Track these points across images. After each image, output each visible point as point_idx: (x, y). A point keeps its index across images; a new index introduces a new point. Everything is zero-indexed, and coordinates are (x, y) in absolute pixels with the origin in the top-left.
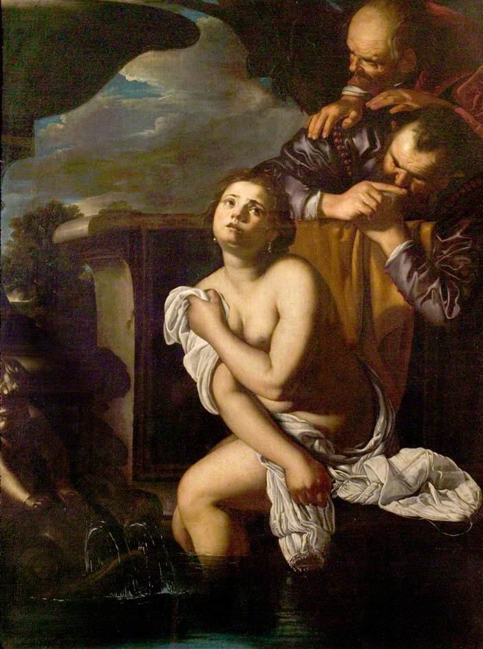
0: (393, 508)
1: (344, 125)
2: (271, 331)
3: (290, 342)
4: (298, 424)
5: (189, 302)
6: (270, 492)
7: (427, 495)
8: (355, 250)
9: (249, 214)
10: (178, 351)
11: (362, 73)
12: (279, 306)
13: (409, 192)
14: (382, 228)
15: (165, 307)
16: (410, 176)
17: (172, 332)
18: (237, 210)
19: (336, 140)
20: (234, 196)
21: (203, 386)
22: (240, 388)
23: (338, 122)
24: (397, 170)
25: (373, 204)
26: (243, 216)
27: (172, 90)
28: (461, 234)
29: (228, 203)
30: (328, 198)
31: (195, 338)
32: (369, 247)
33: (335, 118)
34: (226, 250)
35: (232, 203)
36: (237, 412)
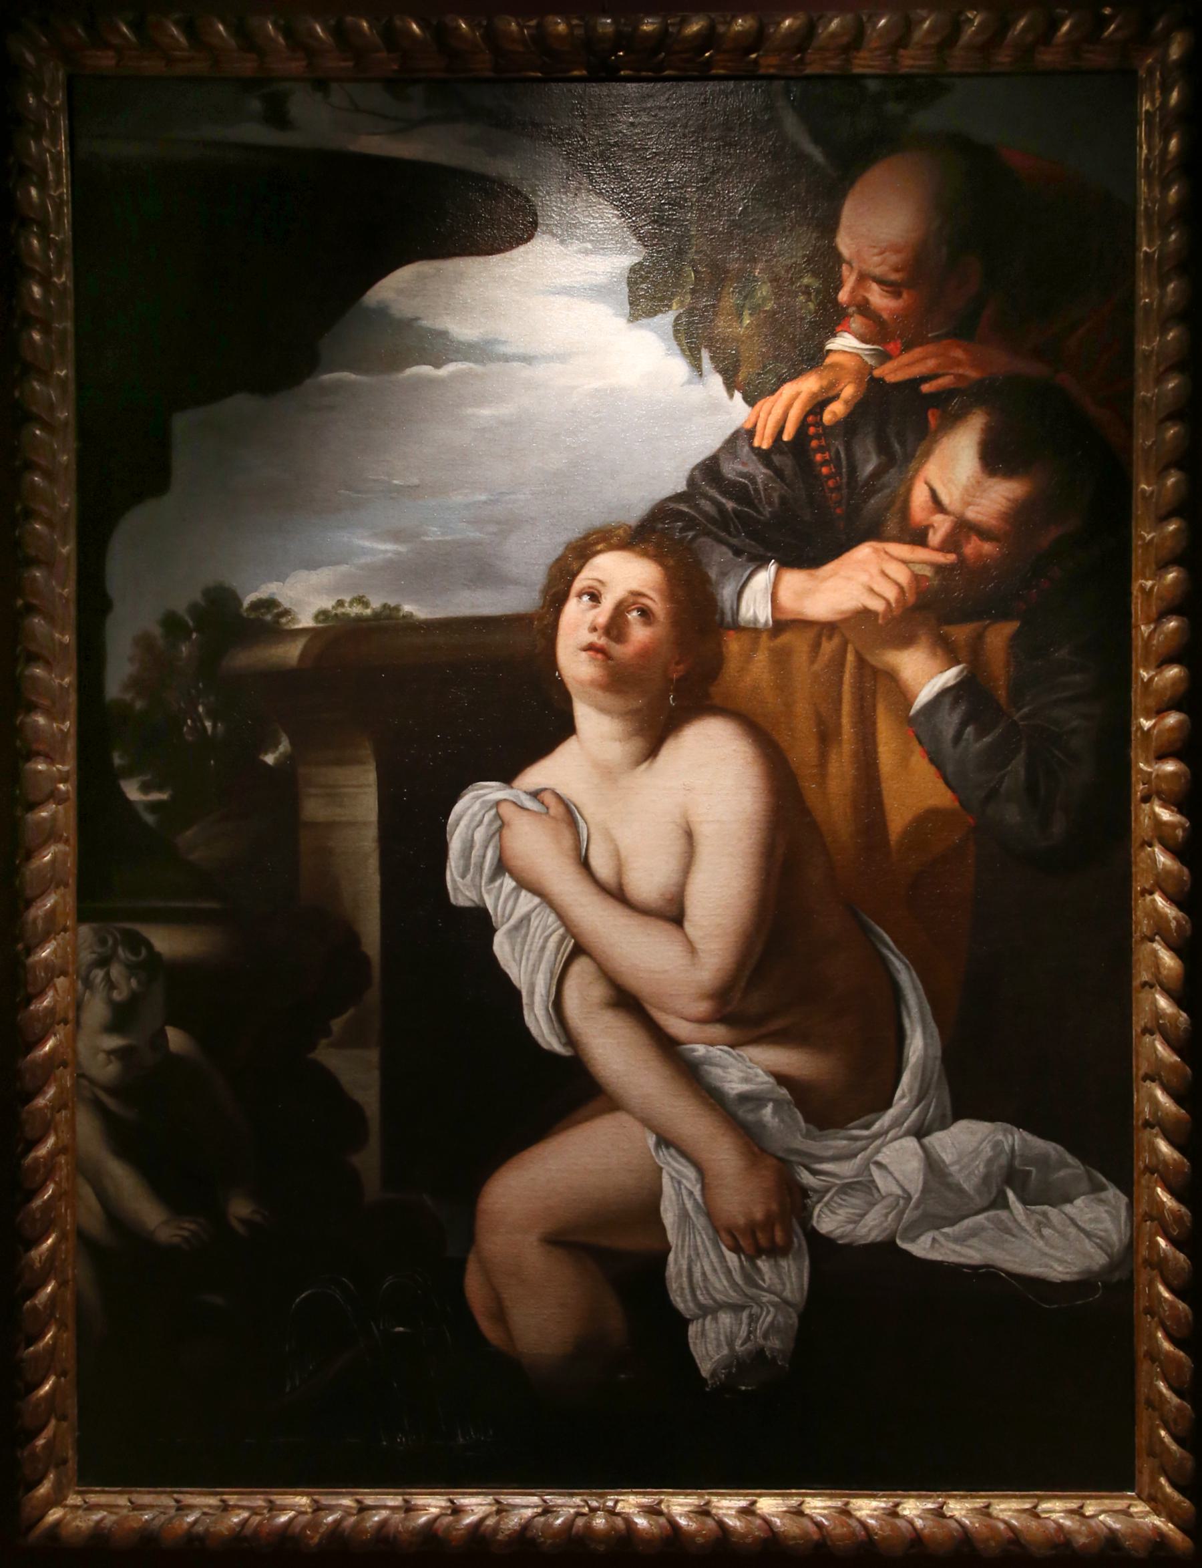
0: (921, 1248)
1: (827, 417)
2: (675, 877)
3: (721, 893)
4: (743, 1069)
5: (498, 816)
6: (669, 1217)
7: (1003, 1214)
8: (847, 677)
9: (627, 621)
10: (479, 923)
11: (864, 308)
12: (694, 819)
13: (962, 559)
14: (906, 641)
16: (963, 528)
19: (814, 443)
20: (600, 581)
21: (538, 999)
22: (626, 1001)
23: (818, 405)
24: (938, 518)
25: (891, 593)
26: (615, 628)
28: (734, 510)
29: (586, 598)
30: (794, 580)
32: (877, 684)
33: (814, 395)
35: (595, 597)
36: (613, 1050)
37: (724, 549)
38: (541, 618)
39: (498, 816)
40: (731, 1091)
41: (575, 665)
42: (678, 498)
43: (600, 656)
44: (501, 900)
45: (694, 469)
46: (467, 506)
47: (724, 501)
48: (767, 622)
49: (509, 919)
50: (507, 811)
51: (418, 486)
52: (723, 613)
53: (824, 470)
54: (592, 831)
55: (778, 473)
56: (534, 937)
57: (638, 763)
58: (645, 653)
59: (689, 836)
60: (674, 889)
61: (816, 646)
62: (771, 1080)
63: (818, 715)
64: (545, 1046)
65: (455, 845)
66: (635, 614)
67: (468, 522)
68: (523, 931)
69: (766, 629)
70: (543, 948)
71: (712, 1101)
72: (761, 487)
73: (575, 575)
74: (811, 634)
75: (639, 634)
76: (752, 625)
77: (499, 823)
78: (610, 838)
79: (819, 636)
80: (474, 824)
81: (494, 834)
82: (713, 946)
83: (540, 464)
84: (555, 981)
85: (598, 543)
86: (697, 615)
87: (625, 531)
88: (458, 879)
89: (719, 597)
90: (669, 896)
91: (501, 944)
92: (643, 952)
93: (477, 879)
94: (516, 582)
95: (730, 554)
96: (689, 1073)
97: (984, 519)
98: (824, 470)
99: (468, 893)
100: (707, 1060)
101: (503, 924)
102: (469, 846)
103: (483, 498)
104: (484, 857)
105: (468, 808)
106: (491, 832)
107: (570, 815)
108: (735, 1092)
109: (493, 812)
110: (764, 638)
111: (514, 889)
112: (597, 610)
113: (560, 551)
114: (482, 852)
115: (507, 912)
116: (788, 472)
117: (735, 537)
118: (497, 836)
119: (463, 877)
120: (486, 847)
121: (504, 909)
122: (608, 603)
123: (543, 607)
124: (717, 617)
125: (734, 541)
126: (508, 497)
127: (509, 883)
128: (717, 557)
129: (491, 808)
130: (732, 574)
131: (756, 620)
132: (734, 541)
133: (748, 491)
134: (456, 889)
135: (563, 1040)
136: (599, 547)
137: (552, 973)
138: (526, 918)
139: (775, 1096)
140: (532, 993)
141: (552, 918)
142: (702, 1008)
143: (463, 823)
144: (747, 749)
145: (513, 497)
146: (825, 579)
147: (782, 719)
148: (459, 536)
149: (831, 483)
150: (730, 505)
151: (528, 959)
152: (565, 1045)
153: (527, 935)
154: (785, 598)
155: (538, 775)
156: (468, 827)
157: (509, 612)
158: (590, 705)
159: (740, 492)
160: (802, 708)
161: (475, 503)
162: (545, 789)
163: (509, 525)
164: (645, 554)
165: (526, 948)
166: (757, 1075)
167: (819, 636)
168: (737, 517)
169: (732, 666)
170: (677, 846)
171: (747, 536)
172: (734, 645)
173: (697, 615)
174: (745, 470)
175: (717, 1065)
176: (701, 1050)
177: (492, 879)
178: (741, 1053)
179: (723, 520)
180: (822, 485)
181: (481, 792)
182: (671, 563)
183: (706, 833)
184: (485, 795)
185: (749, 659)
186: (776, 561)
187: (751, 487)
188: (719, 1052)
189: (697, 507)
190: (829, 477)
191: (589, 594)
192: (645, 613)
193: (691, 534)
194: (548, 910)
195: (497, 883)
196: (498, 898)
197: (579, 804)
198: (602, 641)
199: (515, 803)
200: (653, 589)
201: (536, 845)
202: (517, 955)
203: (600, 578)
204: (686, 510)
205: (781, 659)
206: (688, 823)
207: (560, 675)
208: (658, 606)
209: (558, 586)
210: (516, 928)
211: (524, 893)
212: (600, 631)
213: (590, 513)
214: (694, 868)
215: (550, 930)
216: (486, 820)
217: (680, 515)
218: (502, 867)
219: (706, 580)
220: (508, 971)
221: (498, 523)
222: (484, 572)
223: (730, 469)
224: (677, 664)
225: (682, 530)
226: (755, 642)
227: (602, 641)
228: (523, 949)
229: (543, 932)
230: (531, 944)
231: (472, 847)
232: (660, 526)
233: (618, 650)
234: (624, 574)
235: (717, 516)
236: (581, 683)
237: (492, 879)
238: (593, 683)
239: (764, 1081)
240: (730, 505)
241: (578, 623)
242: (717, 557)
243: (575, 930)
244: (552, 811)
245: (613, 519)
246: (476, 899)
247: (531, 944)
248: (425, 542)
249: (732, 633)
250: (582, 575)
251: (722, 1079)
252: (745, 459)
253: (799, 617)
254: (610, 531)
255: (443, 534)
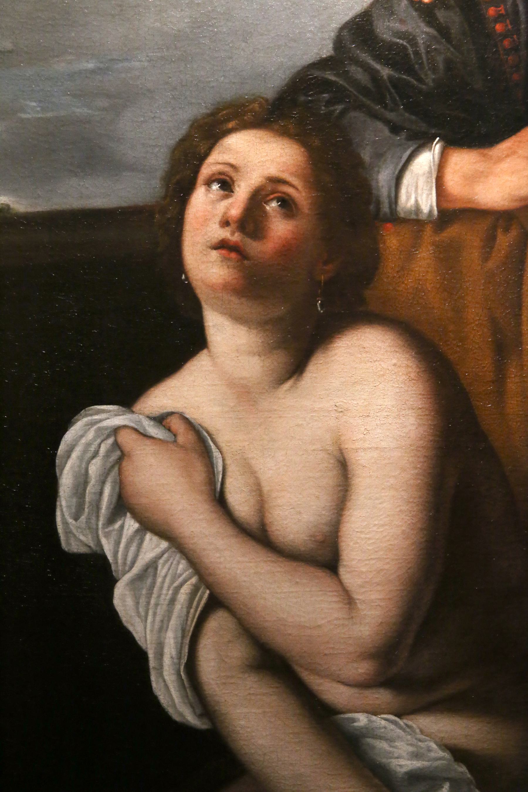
2: (327, 516)
3: (381, 531)
5: (116, 445)
10: (97, 572)
12: (348, 445)
15: (58, 475)
17: (78, 524)
18: (236, 204)
20: (232, 166)
21: (167, 661)
26: (252, 220)
27: (217, 409)
28: (390, 78)
29: (215, 187)
30: (463, 161)
31: (153, 668)
34: (215, 308)
35: (227, 185)
37: (379, 125)
38: (163, 211)
39: (116, 445)
40: (399, 769)
41: (204, 266)
42: (322, 64)
43: (233, 255)
44: (122, 545)
45: (342, 29)
46: (71, 76)
47: (378, 67)
48: (431, 211)
49: (131, 567)
50: (127, 439)
51: (10, 52)
52: (378, 203)
53: (499, 27)
54: (228, 462)
55: (443, 32)
56: (161, 588)
57: (281, 381)
58: (287, 251)
59: (343, 467)
60: (326, 529)
61: (490, 240)
62: (446, 755)
63: (493, 321)
64: (176, 717)
65: (66, 480)
66: (274, 204)
67: (74, 96)
68: (149, 581)
69: (429, 220)
70: (173, 601)
71: (377, 781)
72: (423, 50)
73: (202, 158)
74: (483, 225)
75: (280, 228)
76: (413, 217)
77: (118, 453)
78: (249, 470)
79: (494, 228)
80: (89, 455)
81: (113, 467)
82: (374, 596)
83: (158, 24)
84: (187, 640)
85: (228, 120)
86: (346, 201)
87: (260, 104)
88: (70, 521)
89: (373, 183)
90: (320, 538)
91: (123, 596)
92: (288, 602)
93: (93, 521)
94: (132, 168)
95: (386, 132)
96: (349, 747)
97: (507, 204)
98: (499, 27)
99: (82, 538)
100: (369, 732)
101: (124, 574)
102: (82, 481)
103: (91, 65)
104: (101, 493)
105: (82, 436)
106: (109, 465)
107: (200, 443)
108: (404, 770)
109: (110, 441)
110: (428, 230)
111: (137, 531)
112: (230, 200)
113: (184, 129)
114: (98, 488)
115: (128, 562)
116: (454, 31)
117: (392, 110)
118: (116, 469)
119: (76, 519)
120: (103, 483)
121: (125, 559)
122: (243, 191)
123: (165, 198)
124: (372, 207)
125: (391, 116)
126: (120, 65)
127: (131, 525)
128: (370, 134)
129: (108, 437)
130: (389, 156)
131: (418, 209)
132: (391, 116)
133: (407, 55)
134: (68, 532)
135: (199, 711)
136: (231, 125)
137: (183, 630)
138: (152, 566)
139: (452, 775)
140: (160, 655)
141: (183, 565)
142: (363, 669)
143: (74, 455)
144: (410, 363)
145: (126, 64)
146: (500, 160)
147: (451, 327)
148: (63, 113)
149: (506, 43)
150: (385, 72)
151: (155, 614)
152: (200, 716)
153: (154, 583)
154: (453, 182)
155: (163, 397)
156: (81, 459)
157: (124, 204)
158: (223, 313)
159: (398, 56)
160: (475, 313)
161: (80, 72)
162: (172, 414)
163: (123, 98)
164: (284, 133)
165: (153, 601)
166: (429, 750)
167: (494, 228)
168: (395, 86)
169: (390, 265)
170: (329, 479)
171: (406, 109)
172: (392, 241)
173: (346, 201)
174: (403, 28)
175: (380, 738)
176: (362, 720)
177: (111, 521)
178: (410, 723)
179: (377, 90)
180: (496, 46)
181: (96, 417)
182: (317, 142)
183: (363, 461)
184: (101, 421)
185: (409, 256)
186: (442, 139)
187: (410, 50)
188: (383, 722)
189: (346, 75)
190: (505, 35)
191: (219, 181)
192: (287, 204)
193: (339, 108)
194: (178, 556)
195: (117, 525)
196: (118, 543)
197: (211, 429)
198: (236, 238)
199: (136, 430)
200: (292, 174)
201: (162, 479)
202: (142, 610)
203: (232, 161)
204: (333, 78)
205: (448, 256)
206: (341, 450)
207: (187, 278)
208: (300, 194)
209: (183, 174)
210: (141, 577)
211: (148, 536)
212: (233, 226)
213: (222, 84)
214: (349, 504)
215: (181, 579)
216: (103, 450)
217: (326, 85)
218: (122, 506)
219: (359, 163)
220: (131, 629)
221: (108, 96)
222: (93, 155)
223: (386, 28)
224: (326, 263)
225: (329, 103)
226: (418, 236)
227: (236, 238)
228: (148, 603)
229: (172, 582)
230: (159, 596)
231: (86, 483)
232: (302, 98)
233: (255, 248)
234: (258, 156)
235: (370, 85)
236: (212, 287)
237: (111, 521)
238: (226, 287)
239: (438, 756)
240: (385, 72)
241: (206, 214)
242: (370, 134)
243: (211, 579)
244: (181, 439)
245: (249, 89)
246: (92, 544)
247: (159, 596)
248: (22, 120)
249: (389, 225)
250: (211, 159)
251: (389, 755)
252: (403, 15)
253: (469, 206)
254: (243, 105)
255: (43, 110)
